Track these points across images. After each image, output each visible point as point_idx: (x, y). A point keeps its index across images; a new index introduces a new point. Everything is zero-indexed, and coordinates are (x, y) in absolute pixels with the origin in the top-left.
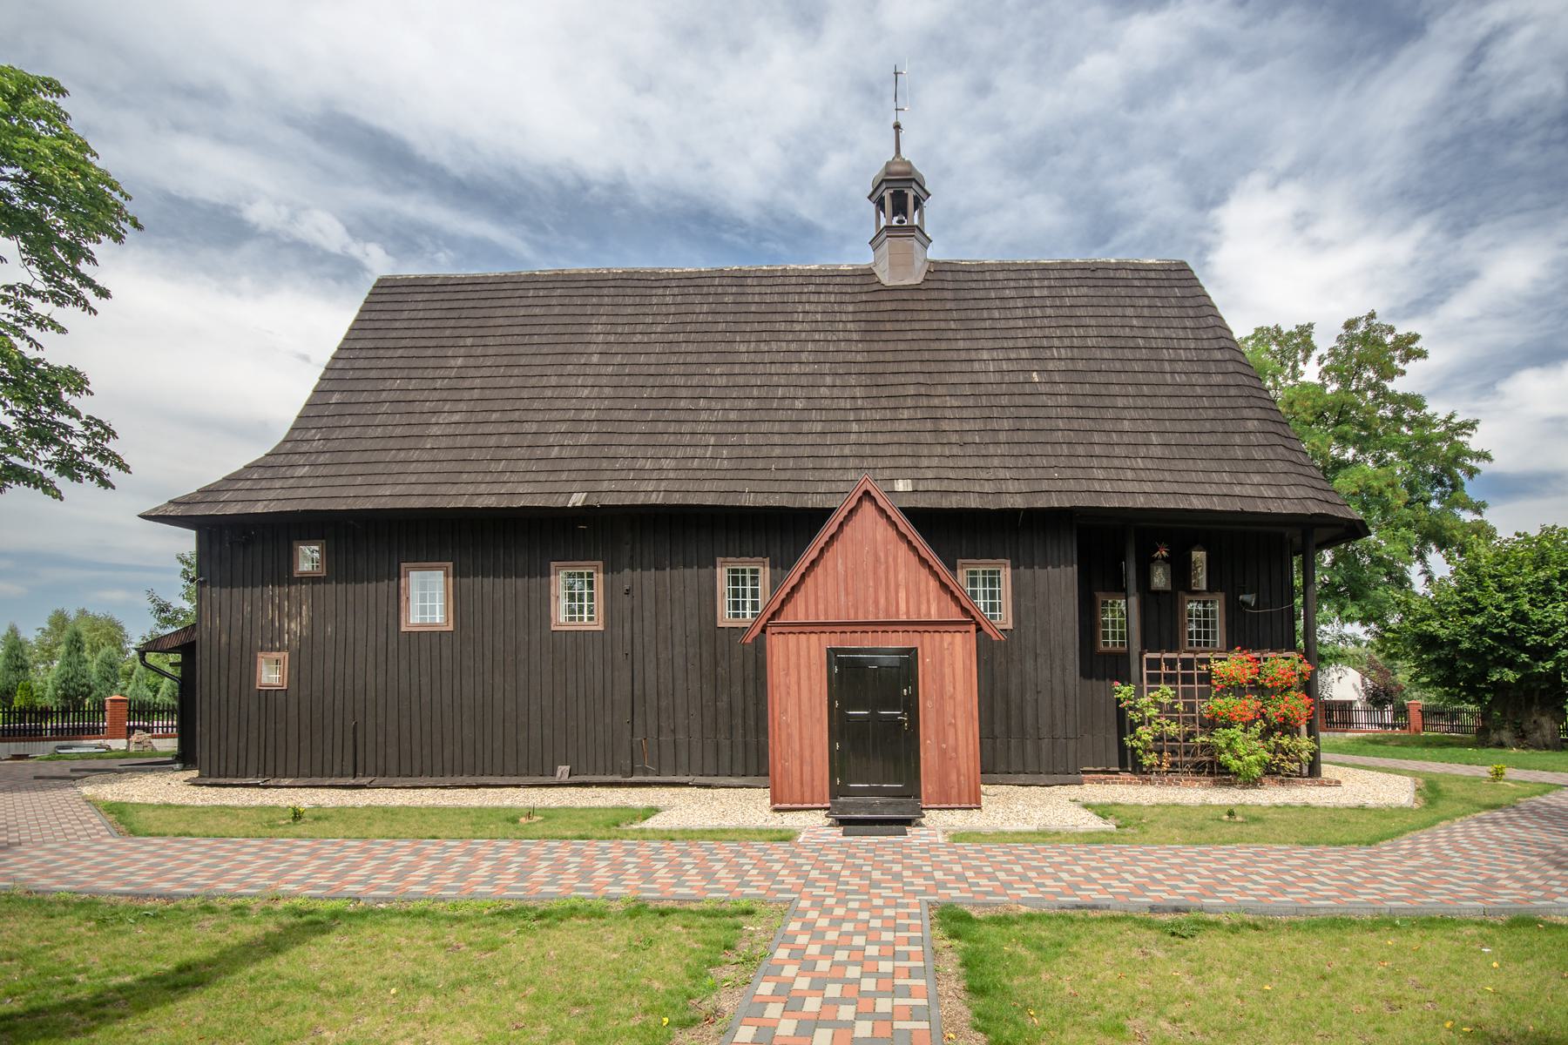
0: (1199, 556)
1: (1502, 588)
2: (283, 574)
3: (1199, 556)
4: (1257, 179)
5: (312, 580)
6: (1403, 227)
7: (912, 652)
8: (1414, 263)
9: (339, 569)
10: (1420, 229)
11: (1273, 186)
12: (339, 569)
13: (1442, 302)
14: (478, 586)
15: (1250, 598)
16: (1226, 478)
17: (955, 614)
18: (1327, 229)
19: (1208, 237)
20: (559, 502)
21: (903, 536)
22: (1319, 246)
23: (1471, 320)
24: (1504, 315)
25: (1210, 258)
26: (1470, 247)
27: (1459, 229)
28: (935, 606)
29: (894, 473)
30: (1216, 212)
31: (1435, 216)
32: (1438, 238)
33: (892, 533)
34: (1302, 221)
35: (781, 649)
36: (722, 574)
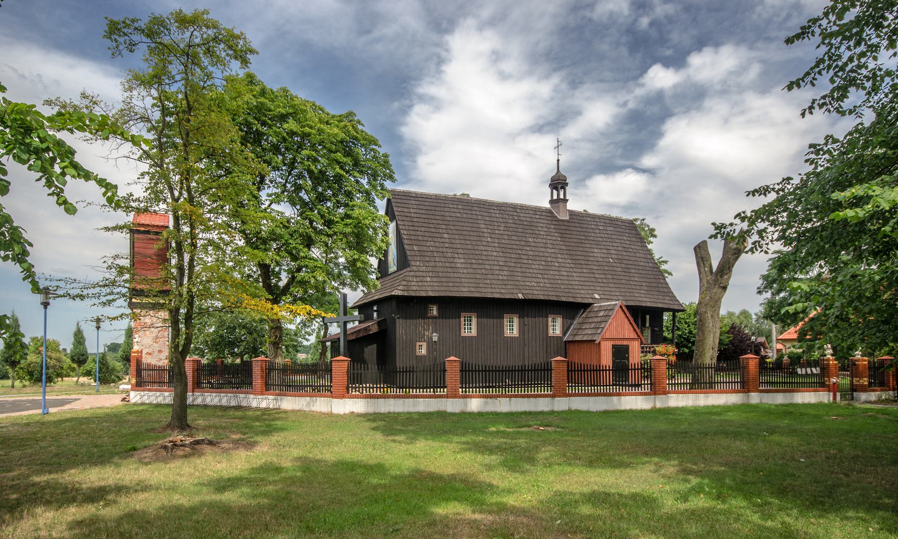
0: (648, 317)
1: (686, 323)
2: (424, 315)
3: (648, 317)
4: (470, 22)
5: (435, 318)
6: (547, 76)
7: (628, 345)
8: (552, 99)
9: (442, 315)
10: (555, 79)
11: (481, 28)
12: (442, 315)
13: (563, 126)
14: (486, 322)
15: (657, 329)
16: (661, 297)
17: (636, 337)
18: (509, 66)
19: (444, 54)
20: (515, 297)
21: (627, 317)
22: (504, 77)
23: (576, 140)
24: (590, 141)
25: (444, 68)
26: (579, 98)
27: (574, 84)
28: (633, 335)
29: (593, 292)
30: (448, 38)
31: (563, 73)
32: (564, 86)
33: (624, 316)
34: (496, 57)
35: (603, 344)
36: (550, 319)
